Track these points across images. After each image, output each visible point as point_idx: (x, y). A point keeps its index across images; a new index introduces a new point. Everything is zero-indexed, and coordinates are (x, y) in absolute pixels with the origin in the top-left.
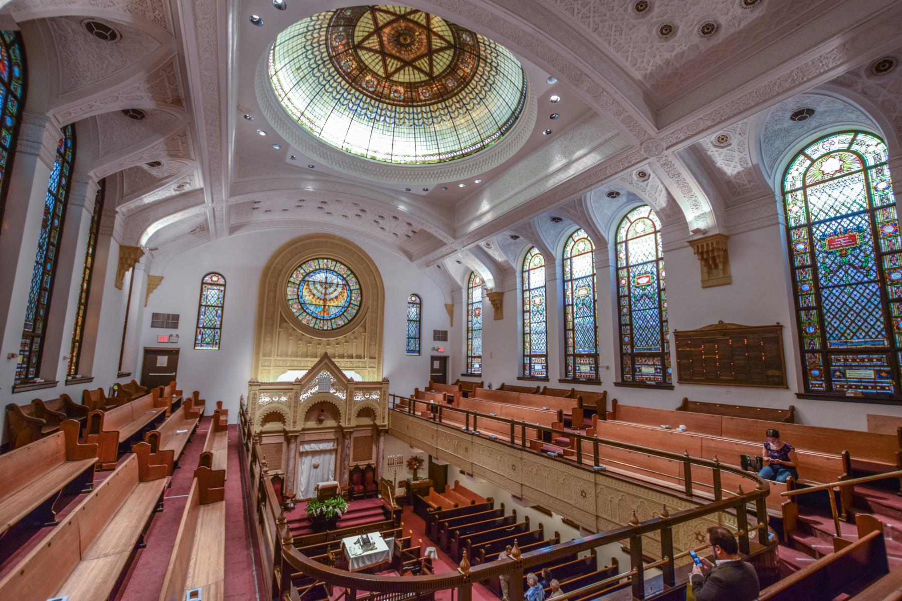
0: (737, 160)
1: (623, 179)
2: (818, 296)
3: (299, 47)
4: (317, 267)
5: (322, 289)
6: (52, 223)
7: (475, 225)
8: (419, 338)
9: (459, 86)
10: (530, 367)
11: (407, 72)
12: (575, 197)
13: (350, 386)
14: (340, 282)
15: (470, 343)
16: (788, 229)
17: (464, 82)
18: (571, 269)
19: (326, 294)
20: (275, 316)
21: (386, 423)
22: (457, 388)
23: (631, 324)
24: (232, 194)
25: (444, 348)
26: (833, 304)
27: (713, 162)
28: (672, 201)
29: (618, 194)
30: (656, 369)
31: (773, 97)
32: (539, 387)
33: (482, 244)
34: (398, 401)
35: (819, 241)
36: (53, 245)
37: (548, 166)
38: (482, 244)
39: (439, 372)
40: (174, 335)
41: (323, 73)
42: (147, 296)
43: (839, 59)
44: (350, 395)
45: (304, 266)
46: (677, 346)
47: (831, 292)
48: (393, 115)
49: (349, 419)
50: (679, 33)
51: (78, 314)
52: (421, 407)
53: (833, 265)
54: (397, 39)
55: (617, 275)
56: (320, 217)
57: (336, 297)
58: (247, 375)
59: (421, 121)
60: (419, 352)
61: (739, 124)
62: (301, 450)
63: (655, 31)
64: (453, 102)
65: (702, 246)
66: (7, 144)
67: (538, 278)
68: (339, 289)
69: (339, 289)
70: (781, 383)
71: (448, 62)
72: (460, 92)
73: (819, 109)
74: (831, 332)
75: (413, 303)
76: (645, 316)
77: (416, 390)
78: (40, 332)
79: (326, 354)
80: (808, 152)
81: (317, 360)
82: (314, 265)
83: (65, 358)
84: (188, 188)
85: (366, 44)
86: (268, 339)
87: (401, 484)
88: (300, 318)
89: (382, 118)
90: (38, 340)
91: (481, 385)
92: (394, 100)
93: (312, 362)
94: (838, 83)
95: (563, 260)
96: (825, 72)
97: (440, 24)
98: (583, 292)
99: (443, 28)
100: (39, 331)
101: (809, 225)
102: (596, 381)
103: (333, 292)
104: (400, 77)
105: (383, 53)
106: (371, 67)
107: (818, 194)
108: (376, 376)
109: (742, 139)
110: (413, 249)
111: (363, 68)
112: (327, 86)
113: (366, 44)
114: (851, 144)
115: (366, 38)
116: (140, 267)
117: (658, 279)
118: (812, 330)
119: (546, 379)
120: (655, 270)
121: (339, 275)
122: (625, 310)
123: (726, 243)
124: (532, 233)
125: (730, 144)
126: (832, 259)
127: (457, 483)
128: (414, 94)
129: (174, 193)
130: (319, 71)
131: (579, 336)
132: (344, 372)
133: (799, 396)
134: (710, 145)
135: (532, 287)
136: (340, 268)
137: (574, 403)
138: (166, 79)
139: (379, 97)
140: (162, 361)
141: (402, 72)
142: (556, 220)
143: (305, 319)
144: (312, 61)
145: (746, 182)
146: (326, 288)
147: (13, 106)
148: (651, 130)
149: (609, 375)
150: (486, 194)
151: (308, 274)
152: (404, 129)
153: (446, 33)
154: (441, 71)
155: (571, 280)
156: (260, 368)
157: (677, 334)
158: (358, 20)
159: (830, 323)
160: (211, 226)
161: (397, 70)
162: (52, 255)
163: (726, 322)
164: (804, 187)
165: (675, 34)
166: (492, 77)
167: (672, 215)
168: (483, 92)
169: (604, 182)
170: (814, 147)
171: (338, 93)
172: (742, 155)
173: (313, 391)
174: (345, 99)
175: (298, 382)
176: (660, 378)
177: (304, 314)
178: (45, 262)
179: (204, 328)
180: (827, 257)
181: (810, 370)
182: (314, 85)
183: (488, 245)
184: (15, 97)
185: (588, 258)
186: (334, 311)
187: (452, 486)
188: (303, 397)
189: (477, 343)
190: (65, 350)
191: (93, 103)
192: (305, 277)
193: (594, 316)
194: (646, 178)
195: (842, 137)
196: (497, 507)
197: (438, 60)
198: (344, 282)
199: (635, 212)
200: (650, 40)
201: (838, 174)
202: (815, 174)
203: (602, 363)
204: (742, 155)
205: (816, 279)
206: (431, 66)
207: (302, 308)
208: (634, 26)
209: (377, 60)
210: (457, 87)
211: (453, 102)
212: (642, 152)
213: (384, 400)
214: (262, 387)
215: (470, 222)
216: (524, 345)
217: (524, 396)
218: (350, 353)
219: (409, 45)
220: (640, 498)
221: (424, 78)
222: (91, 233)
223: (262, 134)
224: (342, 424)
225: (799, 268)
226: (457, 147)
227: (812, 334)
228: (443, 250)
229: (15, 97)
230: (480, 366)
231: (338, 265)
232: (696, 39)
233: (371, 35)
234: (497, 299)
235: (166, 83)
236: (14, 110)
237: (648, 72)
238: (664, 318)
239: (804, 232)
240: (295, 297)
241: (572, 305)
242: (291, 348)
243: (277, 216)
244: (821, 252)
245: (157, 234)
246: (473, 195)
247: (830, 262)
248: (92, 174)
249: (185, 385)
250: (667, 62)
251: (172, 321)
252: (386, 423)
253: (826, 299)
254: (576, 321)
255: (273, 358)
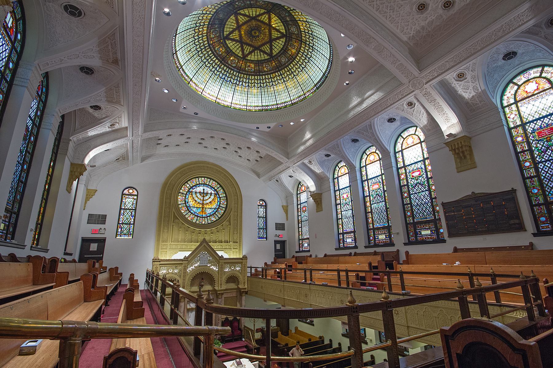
0: (471, 88)
1: (397, 108)
2: (537, 169)
3: (191, 36)
4: (198, 183)
5: (201, 200)
6: (30, 138)
7: (302, 148)
8: (266, 229)
9: (289, 60)
10: (343, 240)
11: (256, 54)
12: (367, 123)
13: (221, 261)
14: (213, 192)
15: (300, 230)
16: (510, 129)
17: (292, 58)
18: (366, 173)
19: (203, 200)
20: (170, 215)
21: (246, 287)
22: (294, 260)
23: (411, 203)
24: (145, 131)
25: (284, 235)
26: (547, 172)
27: (456, 91)
28: (432, 120)
29: (395, 119)
30: (431, 231)
31: (492, 43)
32: (351, 253)
33: (306, 161)
34: (253, 271)
35: (531, 134)
36: (22, 182)
37: (349, 104)
38: (306, 161)
39: (280, 251)
40: (103, 229)
41: (205, 55)
42: (86, 203)
43: (530, 16)
44: (221, 268)
45: (189, 182)
46: (445, 213)
47: (545, 165)
48: (247, 81)
49: (221, 284)
50: (430, 8)
51: (41, 205)
52: (271, 272)
53: (543, 148)
54: (249, 33)
55: (398, 173)
56: (200, 150)
57: (210, 202)
58: (151, 256)
59: (265, 84)
60: (266, 238)
61: (470, 63)
62: (188, 307)
63: (415, 8)
64: (285, 71)
65: (454, 145)
66: (8, 79)
67: (344, 181)
68: (212, 197)
69: (212, 197)
70: (521, 228)
71: (282, 46)
72: (289, 64)
73: (520, 52)
74: (549, 190)
75: (261, 205)
76: (420, 197)
77: (266, 264)
78: (16, 211)
79: (204, 239)
80: (515, 81)
81: (198, 244)
82: (195, 181)
83: (31, 230)
84: (117, 126)
85: (231, 36)
86: (166, 231)
87: (258, 331)
88: (187, 216)
89: (241, 83)
90: (14, 216)
91: (311, 256)
92: (248, 72)
93: (194, 246)
94: (530, 32)
95: (361, 168)
96: (523, 24)
97: (277, 22)
98: (376, 187)
99: (279, 24)
100: (16, 210)
101: (523, 125)
102: (392, 244)
103: (208, 199)
104: (251, 57)
105: (241, 42)
106: (234, 51)
107: (526, 105)
108: (238, 255)
109: (473, 74)
110: (260, 170)
111: (229, 52)
112: (207, 63)
113: (231, 36)
114: (541, 73)
115: (231, 33)
116: (83, 178)
117: (426, 172)
118: (536, 191)
119: (356, 247)
120: (423, 166)
121: (212, 188)
122: (406, 195)
123: (469, 142)
124: (340, 151)
125: (466, 78)
126: (542, 144)
127: (296, 328)
128: (260, 67)
129: (108, 130)
130: (202, 53)
131: (376, 216)
132: (217, 252)
133: (535, 235)
134: (453, 80)
135: (340, 188)
136: (214, 184)
137: (379, 258)
138: (110, 45)
139: (240, 70)
140: (94, 247)
141: (253, 54)
142: (355, 141)
143: (189, 217)
144: (198, 47)
145: (478, 102)
146: (203, 196)
147: (14, 56)
148: (416, 72)
149: (399, 239)
150: (308, 127)
151: (192, 188)
152: (255, 91)
153: (281, 28)
154: (277, 52)
155: (367, 180)
156: (160, 250)
157: (443, 204)
158: (227, 21)
159: (547, 185)
160: (130, 155)
161: (250, 53)
162: (28, 160)
163: (477, 192)
164: (516, 102)
165: (427, 9)
166: (309, 53)
167: (433, 128)
168: (304, 64)
169: (386, 110)
170: (518, 78)
171: (213, 67)
172: (474, 84)
173: (196, 265)
174: (218, 71)
175: (186, 259)
176: (435, 237)
177: (190, 214)
178: (23, 163)
179: (122, 224)
180: (538, 143)
181: (539, 217)
182: (199, 62)
183: (311, 162)
184: (16, 51)
185: (377, 164)
186: (209, 211)
187: (293, 331)
188: (190, 269)
189: (305, 229)
190: (32, 225)
191: (62, 58)
192: (189, 189)
193: (385, 201)
194: (413, 106)
195: (535, 70)
196: (327, 342)
197: (275, 46)
198: (216, 192)
199: (406, 132)
200: (411, 15)
201: (536, 92)
202: (521, 94)
203: (393, 231)
204: (474, 84)
205: (533, 158)
206: (271, 49)
207: (188, 210)
208: (402, 6)
209: (238, 47)
210: (287, 62)
211: (285, 71)
212: (411, 88)
213: (245, 270)
214: (161, 263)
215: (298, 147)
216: (338, 227)
217: (341, 259)
218: (220, 239)
219: (258, 36)
220: (439, 307)
221: (267, 57)
222: (53, 152)
223: (166, 91)
224: (216, 288)
225: (520, 152)
226: (288, 99)
227: (536, 193)
228: (281, 167)
229: (16, 51)
230: (309, 245)
231: (212, 181)
232: (440, 11)
233: (234, 30)
234: (317, 197)
235: (110, 47)
236: (15, 59)
237: (411, 35)
238: (433, 196)
239: (520, 130)
240: (184, 202)
241: (369, 196)
242: (181, 236)
243: (172, 150)
244: (533, 141)
245: (94, 157)
246: (300, 130)
247: (541, 146)
248: (57, 108)
249: (108, 261)
250: (423, 28)
251: (102, 219)
252: (246, 287)
253: (542, 169)
254: (373, 206)
255: (168, 244)
